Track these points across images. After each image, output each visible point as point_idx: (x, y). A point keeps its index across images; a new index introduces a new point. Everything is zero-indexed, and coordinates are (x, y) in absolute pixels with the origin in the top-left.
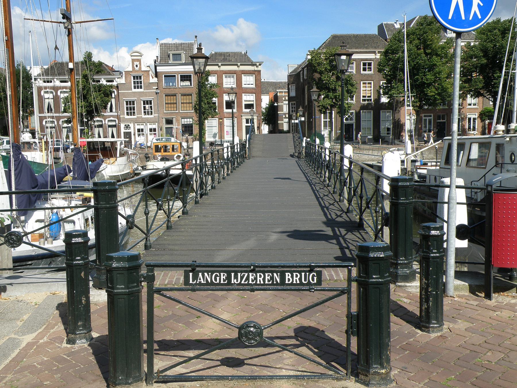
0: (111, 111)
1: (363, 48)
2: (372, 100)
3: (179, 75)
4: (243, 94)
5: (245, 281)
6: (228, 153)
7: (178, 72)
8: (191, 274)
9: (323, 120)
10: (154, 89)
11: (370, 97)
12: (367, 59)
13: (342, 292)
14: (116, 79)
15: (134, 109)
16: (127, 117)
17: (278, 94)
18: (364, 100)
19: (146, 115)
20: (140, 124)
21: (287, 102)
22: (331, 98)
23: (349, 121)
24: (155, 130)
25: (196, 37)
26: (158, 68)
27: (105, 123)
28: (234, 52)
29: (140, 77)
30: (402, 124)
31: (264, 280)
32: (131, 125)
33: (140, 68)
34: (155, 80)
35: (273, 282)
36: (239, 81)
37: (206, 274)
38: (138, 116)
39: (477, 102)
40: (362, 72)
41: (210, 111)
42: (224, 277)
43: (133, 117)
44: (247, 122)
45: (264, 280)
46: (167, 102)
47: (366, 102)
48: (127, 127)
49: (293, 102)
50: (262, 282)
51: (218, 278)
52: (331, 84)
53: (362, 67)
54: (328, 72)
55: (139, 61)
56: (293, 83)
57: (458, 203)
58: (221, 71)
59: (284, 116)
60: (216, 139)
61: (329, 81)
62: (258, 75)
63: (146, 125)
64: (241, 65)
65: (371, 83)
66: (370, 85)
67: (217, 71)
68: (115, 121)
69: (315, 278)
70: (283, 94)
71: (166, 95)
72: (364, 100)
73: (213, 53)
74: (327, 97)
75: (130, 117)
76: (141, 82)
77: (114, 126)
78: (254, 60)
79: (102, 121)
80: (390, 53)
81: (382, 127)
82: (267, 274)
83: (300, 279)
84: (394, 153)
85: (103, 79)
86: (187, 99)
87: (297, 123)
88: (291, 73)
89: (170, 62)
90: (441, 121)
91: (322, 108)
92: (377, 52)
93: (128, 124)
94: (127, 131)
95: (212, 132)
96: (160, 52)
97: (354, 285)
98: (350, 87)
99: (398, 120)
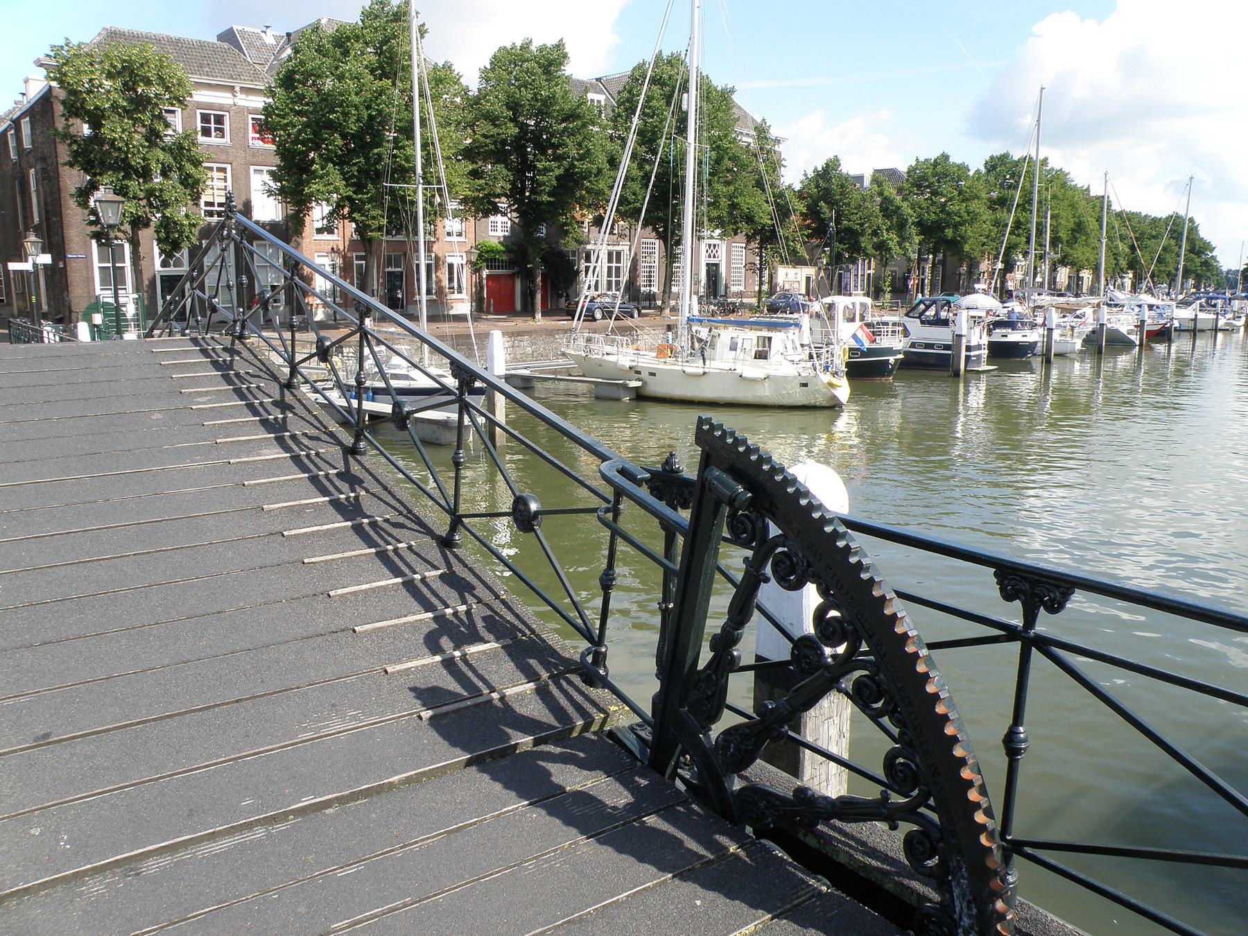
18: (210, 214)
22: (134, 198)
39: (464, 229)
47: (215, 219)
53: (199, 125)
54: (120, 115)
61: (127, 145)
65: (224, 170)
66: (222, 175)
72: (210, 214)
98: (189, 168)
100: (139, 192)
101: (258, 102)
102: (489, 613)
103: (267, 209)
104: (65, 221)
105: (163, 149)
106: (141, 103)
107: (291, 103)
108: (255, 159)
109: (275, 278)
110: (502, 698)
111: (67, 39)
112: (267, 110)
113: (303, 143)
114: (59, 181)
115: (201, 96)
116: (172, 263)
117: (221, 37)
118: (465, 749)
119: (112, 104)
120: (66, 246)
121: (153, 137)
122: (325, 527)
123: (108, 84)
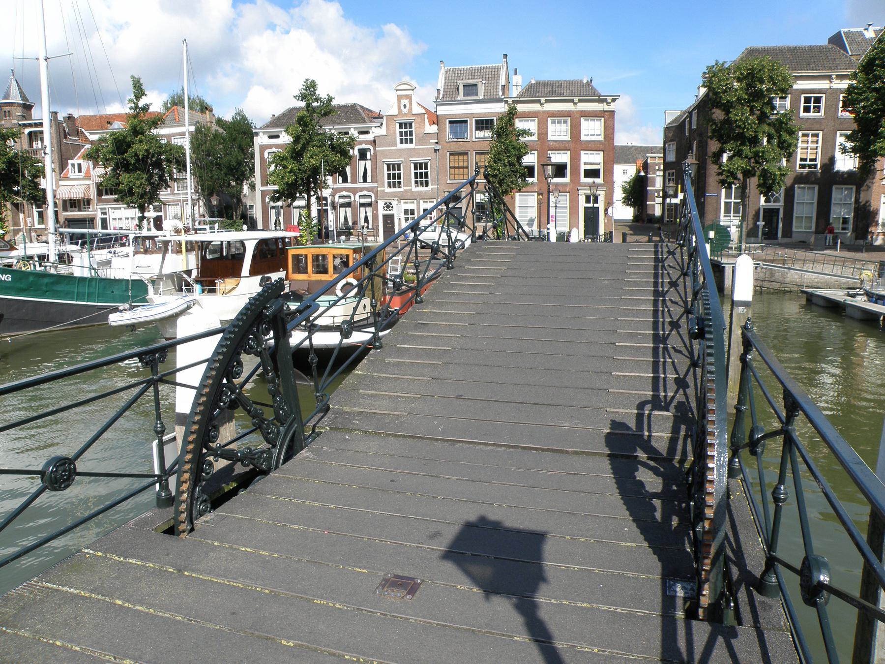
0: (365, 180)
1: (807, 70)
2: (819, 166)
3: (474, 120)
4: (582, 152)
7: (472, 115)
9: (723, 200)
10: (431, 144)
11: (815, 160)
14: (373, 128)
16: (388, 190)
17: (649, 161)
19: (418, 186)
20: (409, 201)
21: (661, 173)
22: (746, 157)
23: (772, 204)
25: (505, 56)
27: (355, 201)
28: (569, 81)
29: (411, 124)
30: (873, 212)
32: (394, 203)
33: (410, 109)
34: (434, 129)
36: (576, 130)
38: (405, 188)
41: (514, 179)
43: (397, 190)
44: (588, 200)
46: (452, 165)
47: (807, 170)
48: (388, 207)
49: (671, 171)
52: (748, 129)
53: (802, 105)
54: (742, 104)
55: (409, 97)
56: (671, 141)
58: (544, 112)
59: (656, 195)
60: (533, 229)
61: (744, 123)
62: (610, 118)
64: (580, 101)
65: (817, 136)
66: (815, 139)
67: (539, 112)
68: (370, 196)
70: (657, 161)
71: (451, 154)
73: (533, 82)
74: (738, 154)
75: (393, 190)
76: (411, 133)
77: (370, 205)
78: (603, 91)
79: (349, 197)
80: (878, 66)
81: (833, 216)
84: (328, 95)
85: (352, 130)
87: (676, 204)
88: (669, 124)
89: (459, 99)
91: (727, 177)
92: (834, 76)
93: (390, 201)
94: (388, 212)
95: (526, 216)
96: (445, 83)
98: (785, 136)
99: (864, 205)
100: (749, 154)
101: (844, 84)
102: (684, 400)
103: (846, 163)
104: (707, 173)
105: (769, 125)
106: (758, 95)
107: (869, 83)
108: (841, 124)
109: (847, 212)
110: (650, 436)
111: (717, 61)
112: (850, 90)
113: (874, 112)
114: (707, 148)
115: (799, 85)
116: (772, 200)
117: (832, 40)
118: (610, 449)
119: (737, 98)
120: (706, 188)
121: (763, 118)
122: (638, 345)
123: (736, 85)
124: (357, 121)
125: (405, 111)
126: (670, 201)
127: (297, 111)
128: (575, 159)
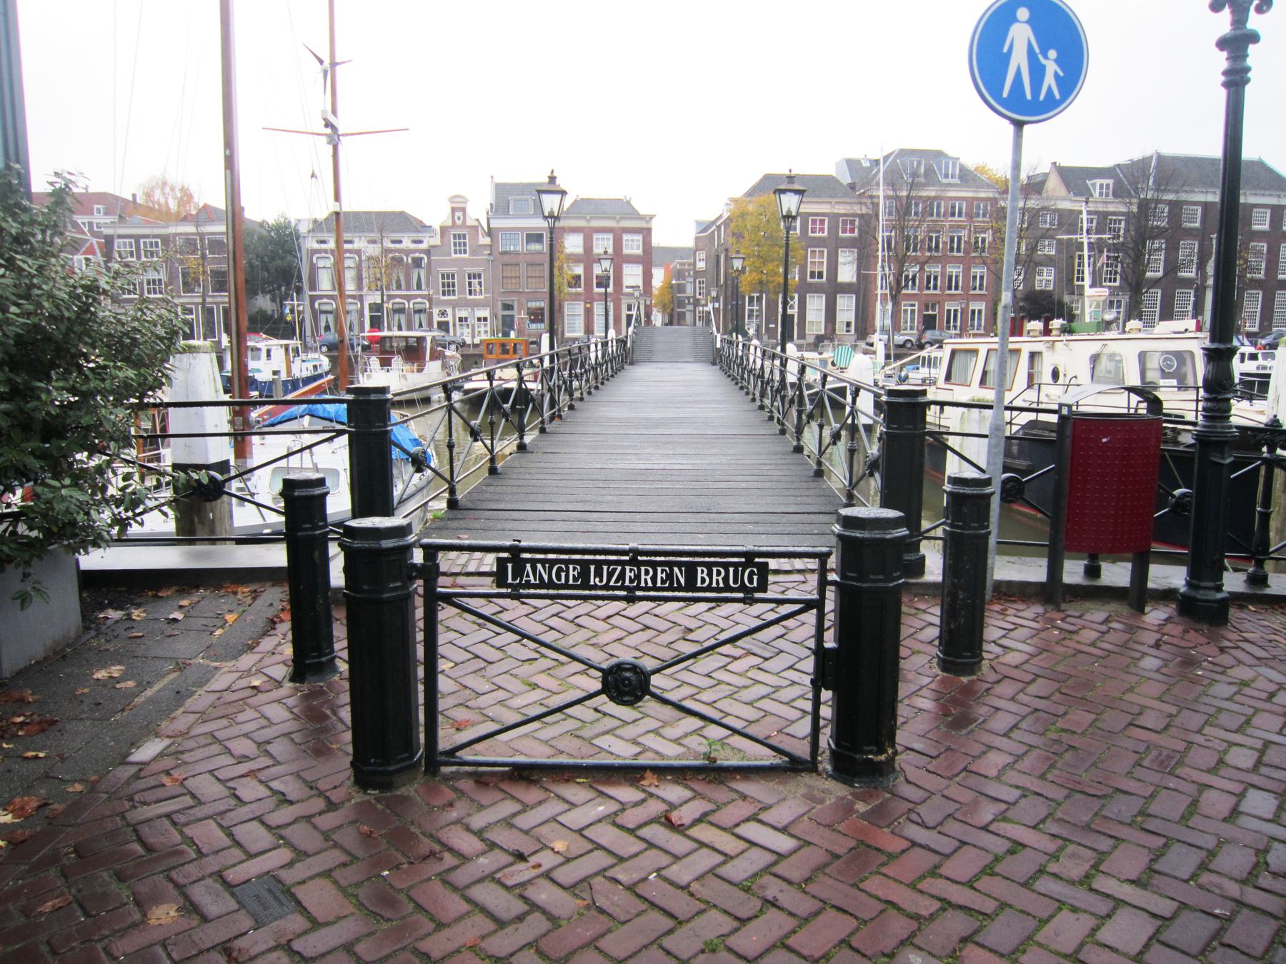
5: (617, 581)
6: (597, 351)
8: (510, 566)
9: (747, 307)
12: (818, 214)
13: (808, 605)
15: (453, 286)
21: (691, 280)
24: (485, 319)
26: (491, 221)
31: (654, 579)
32: (449, 311)
34: (487, 241)
35: (672, 583)
37: (539, 566)
40: (810, 234)
42: (576, 573)
43: (452, 297)
45: (654, 579)
50: (650, 584)
51: (563, 575)
55: (464, 210)
57: (986, 436)
58: (619, 228)
63: (473, 310)
69: (755, 578)
75: (447, 298)
76: (465, 244)
82: (659, 569)
83: (726, 579)
86: (536, 272)
90: (930, 312)
97: (831, 594)
124: (409, 231)
125: (459, 222)
126: (349, 267)
127: (1129, 230)
128: (588, 270)
